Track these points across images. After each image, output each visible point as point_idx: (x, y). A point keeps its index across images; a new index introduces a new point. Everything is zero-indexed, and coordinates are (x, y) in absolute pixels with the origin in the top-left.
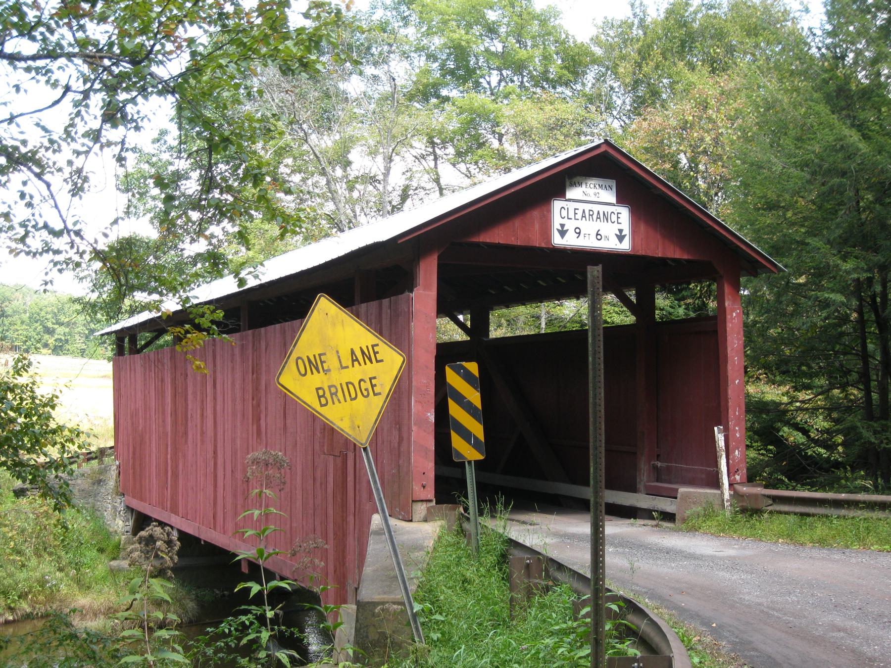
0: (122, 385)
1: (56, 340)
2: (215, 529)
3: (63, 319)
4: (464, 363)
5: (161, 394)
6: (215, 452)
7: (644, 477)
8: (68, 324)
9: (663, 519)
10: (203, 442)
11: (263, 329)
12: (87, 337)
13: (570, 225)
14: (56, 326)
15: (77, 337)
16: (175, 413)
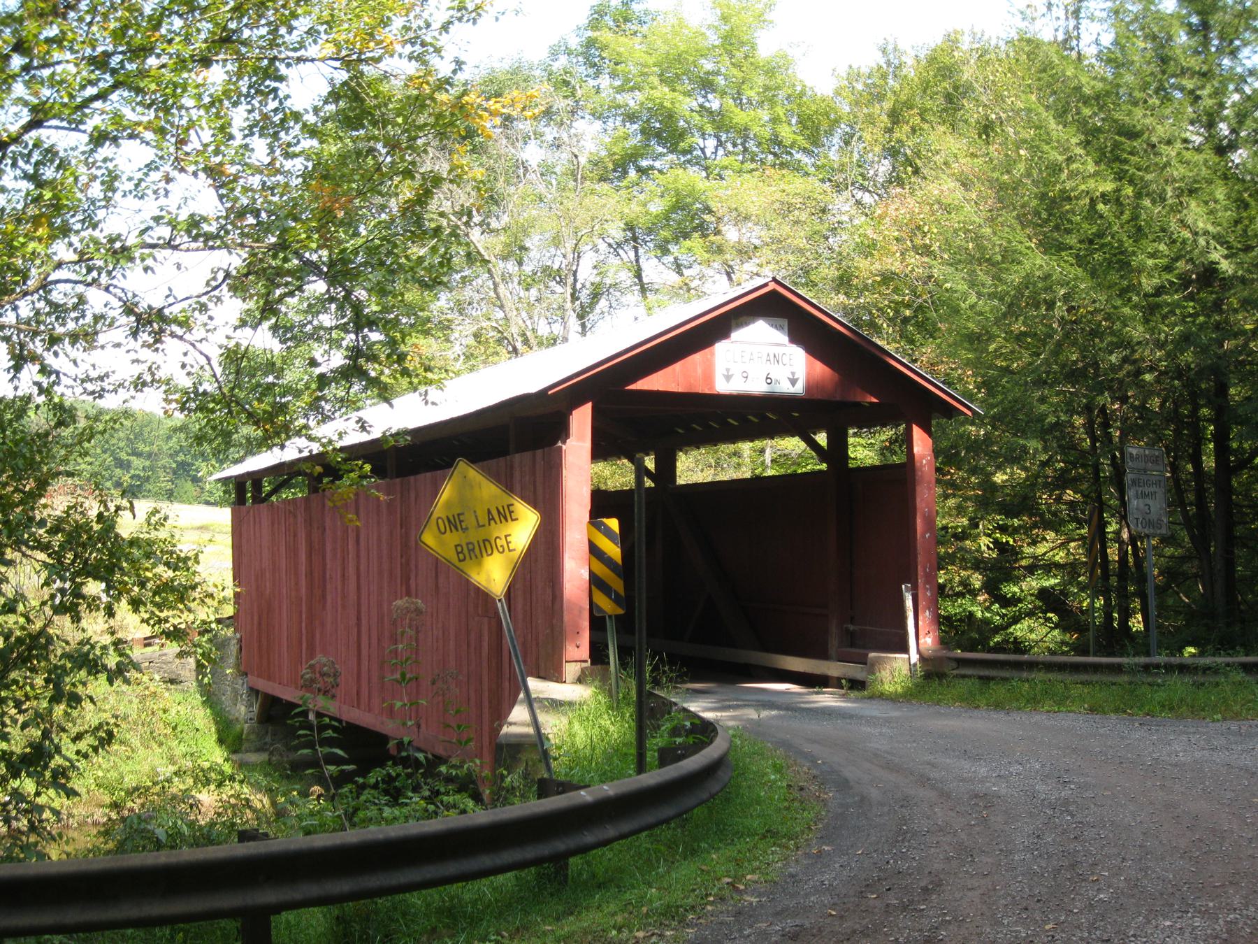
0: (244, 541)
1: (132, 478)
2: (358, 707)
3: (141, 447)
4: (605, 520)
5: (293, 552)
6: (359, 619)
7: (834, 644)
8: (149, 455)
9: (851, 688)
10: (344, 607)
11: (412, 478)
12: (175, 473)
13: (736, 371)
14: (131, 458)
15: (161, 473)
16: (310, 574)
